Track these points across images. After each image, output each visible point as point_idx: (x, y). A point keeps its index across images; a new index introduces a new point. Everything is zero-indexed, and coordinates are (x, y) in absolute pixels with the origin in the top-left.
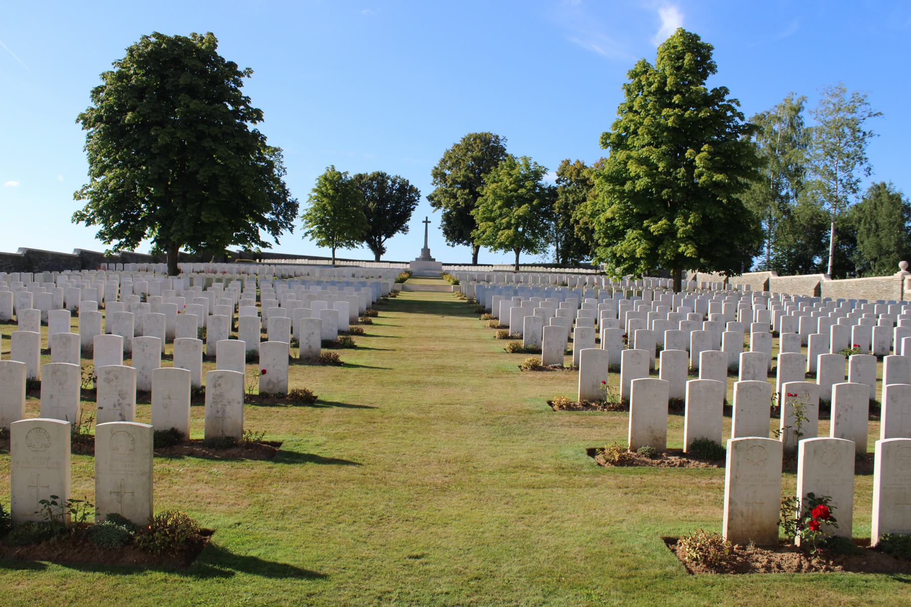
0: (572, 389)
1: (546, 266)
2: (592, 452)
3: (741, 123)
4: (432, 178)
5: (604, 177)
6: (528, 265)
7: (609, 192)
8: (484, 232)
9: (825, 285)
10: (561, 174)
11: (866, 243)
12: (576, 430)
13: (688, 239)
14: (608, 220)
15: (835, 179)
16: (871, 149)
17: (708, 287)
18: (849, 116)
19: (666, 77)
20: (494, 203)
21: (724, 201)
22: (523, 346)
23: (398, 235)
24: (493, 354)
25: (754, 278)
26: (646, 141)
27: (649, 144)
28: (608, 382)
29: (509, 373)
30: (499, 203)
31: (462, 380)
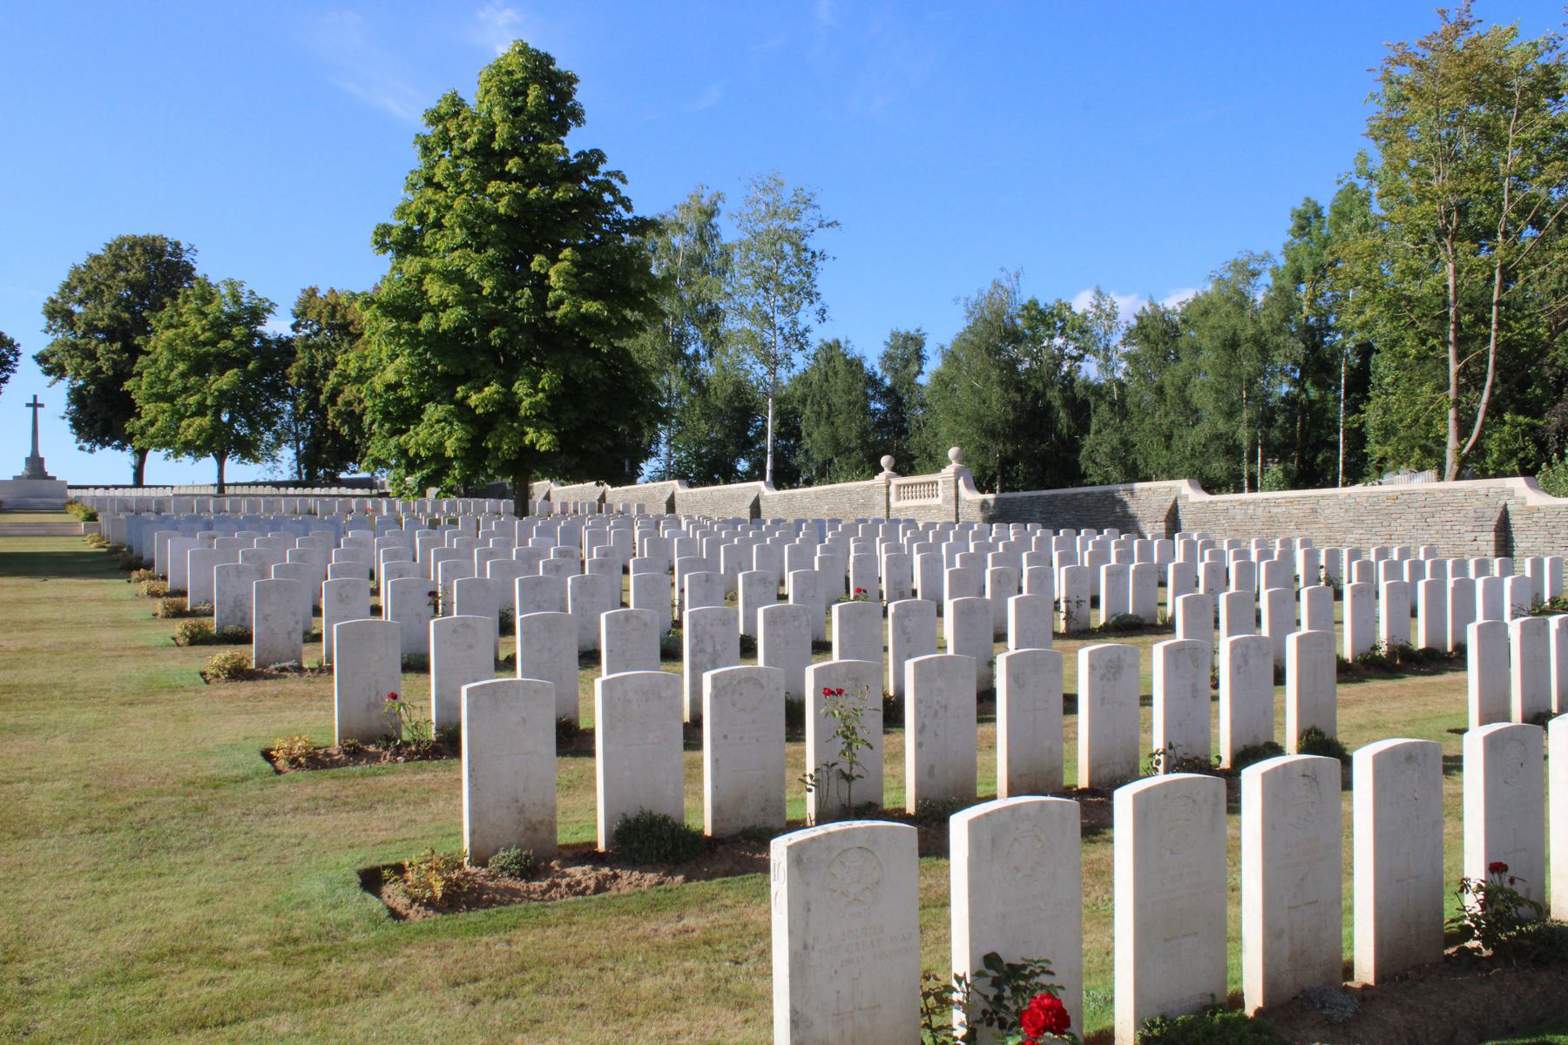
0: (321, 719)
1: (277, 485)
2: (371, 880)
3: (626, 216)
5: (381, 306)
6: (242, 485)
7: (389, 334)
8: (152, 423)
9: (766, 500)
10: (301, 314)
11: (815, 435)
12: (328, 821)
13: (541, 419)
14: (390, 387)
15: (772, 326)
16: (826, 280)
17: (571, 508)
18: (790, 226)
19: (494, 126)
20: (170, 367)
21: (605, 350)
22: (214, 630)
24: (144, 651)
25: (650, 488)
26: (458, 240)
27: (464, 245)
28: (402, 694)
29: (173, 689)
30: (181, 367)
31: (54, 717)
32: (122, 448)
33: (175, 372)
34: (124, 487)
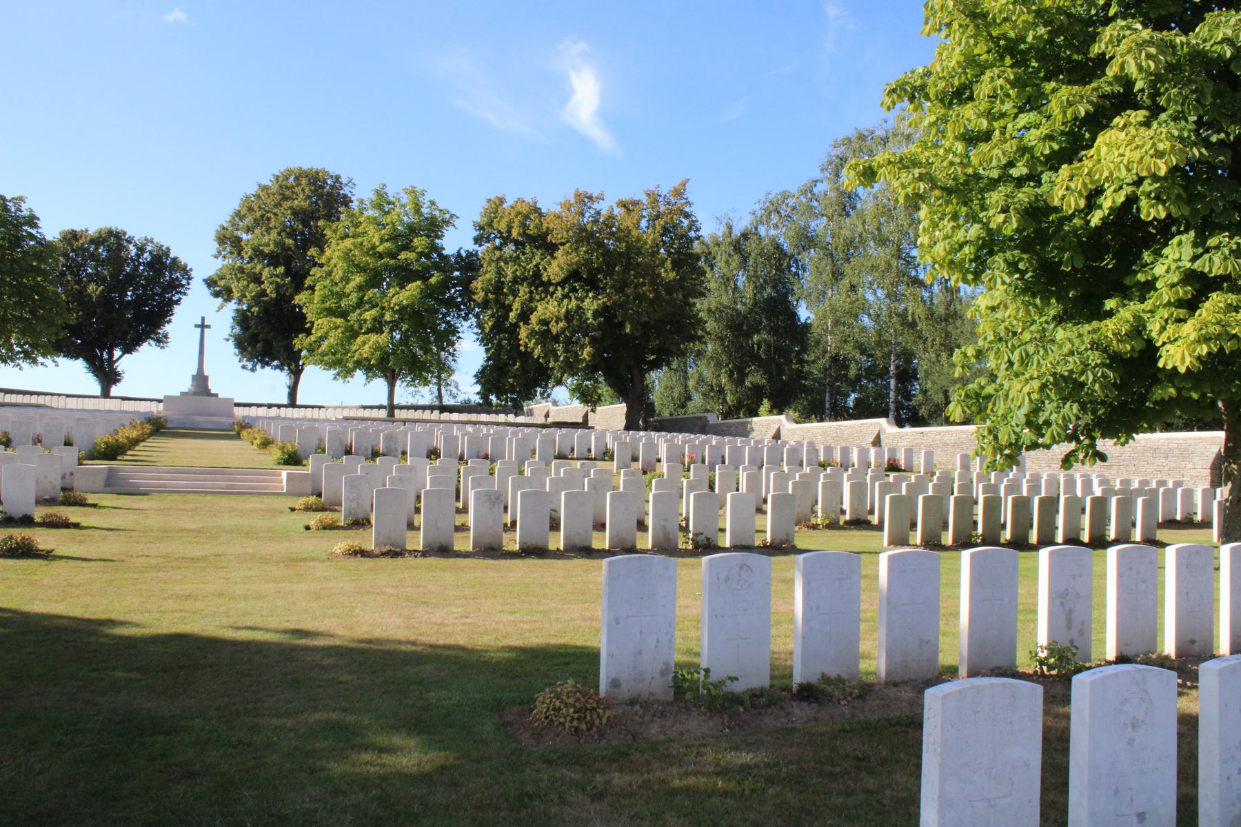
4: (216, 245)
6: (372, 407)
23: (147, 349)
30: (358, 279)
32: (281, 367)
33: (352, 285)
34: (279, 406)
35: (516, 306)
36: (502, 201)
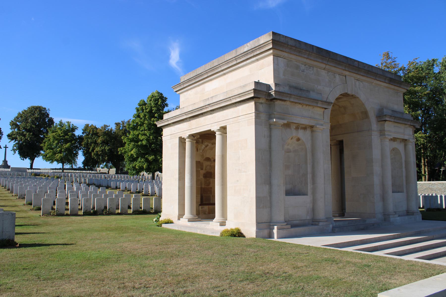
6: (58, 169)
10: (84, 131)
35: (91, 148)
36: (88, 125)
